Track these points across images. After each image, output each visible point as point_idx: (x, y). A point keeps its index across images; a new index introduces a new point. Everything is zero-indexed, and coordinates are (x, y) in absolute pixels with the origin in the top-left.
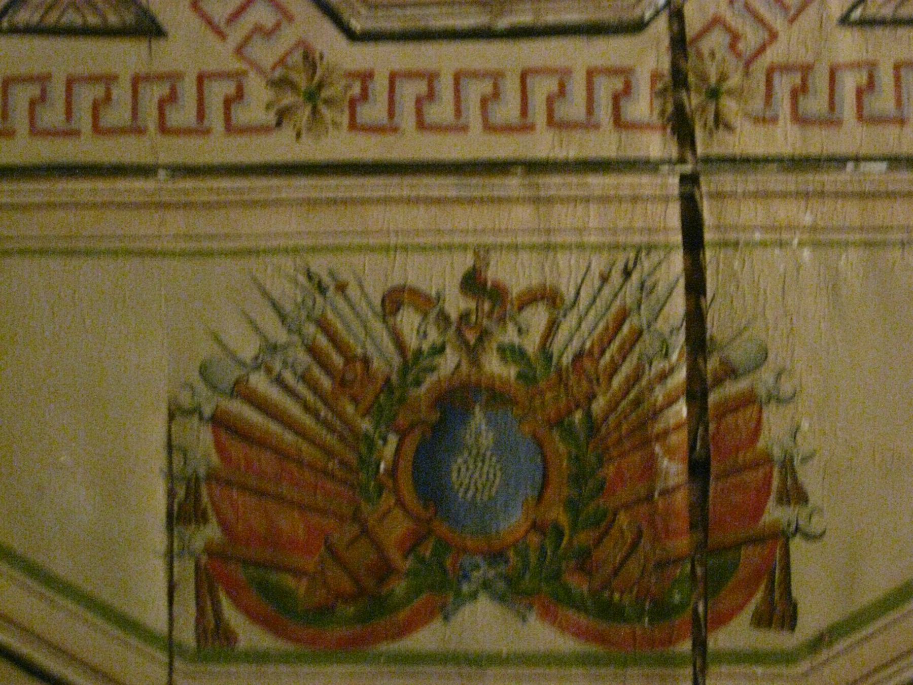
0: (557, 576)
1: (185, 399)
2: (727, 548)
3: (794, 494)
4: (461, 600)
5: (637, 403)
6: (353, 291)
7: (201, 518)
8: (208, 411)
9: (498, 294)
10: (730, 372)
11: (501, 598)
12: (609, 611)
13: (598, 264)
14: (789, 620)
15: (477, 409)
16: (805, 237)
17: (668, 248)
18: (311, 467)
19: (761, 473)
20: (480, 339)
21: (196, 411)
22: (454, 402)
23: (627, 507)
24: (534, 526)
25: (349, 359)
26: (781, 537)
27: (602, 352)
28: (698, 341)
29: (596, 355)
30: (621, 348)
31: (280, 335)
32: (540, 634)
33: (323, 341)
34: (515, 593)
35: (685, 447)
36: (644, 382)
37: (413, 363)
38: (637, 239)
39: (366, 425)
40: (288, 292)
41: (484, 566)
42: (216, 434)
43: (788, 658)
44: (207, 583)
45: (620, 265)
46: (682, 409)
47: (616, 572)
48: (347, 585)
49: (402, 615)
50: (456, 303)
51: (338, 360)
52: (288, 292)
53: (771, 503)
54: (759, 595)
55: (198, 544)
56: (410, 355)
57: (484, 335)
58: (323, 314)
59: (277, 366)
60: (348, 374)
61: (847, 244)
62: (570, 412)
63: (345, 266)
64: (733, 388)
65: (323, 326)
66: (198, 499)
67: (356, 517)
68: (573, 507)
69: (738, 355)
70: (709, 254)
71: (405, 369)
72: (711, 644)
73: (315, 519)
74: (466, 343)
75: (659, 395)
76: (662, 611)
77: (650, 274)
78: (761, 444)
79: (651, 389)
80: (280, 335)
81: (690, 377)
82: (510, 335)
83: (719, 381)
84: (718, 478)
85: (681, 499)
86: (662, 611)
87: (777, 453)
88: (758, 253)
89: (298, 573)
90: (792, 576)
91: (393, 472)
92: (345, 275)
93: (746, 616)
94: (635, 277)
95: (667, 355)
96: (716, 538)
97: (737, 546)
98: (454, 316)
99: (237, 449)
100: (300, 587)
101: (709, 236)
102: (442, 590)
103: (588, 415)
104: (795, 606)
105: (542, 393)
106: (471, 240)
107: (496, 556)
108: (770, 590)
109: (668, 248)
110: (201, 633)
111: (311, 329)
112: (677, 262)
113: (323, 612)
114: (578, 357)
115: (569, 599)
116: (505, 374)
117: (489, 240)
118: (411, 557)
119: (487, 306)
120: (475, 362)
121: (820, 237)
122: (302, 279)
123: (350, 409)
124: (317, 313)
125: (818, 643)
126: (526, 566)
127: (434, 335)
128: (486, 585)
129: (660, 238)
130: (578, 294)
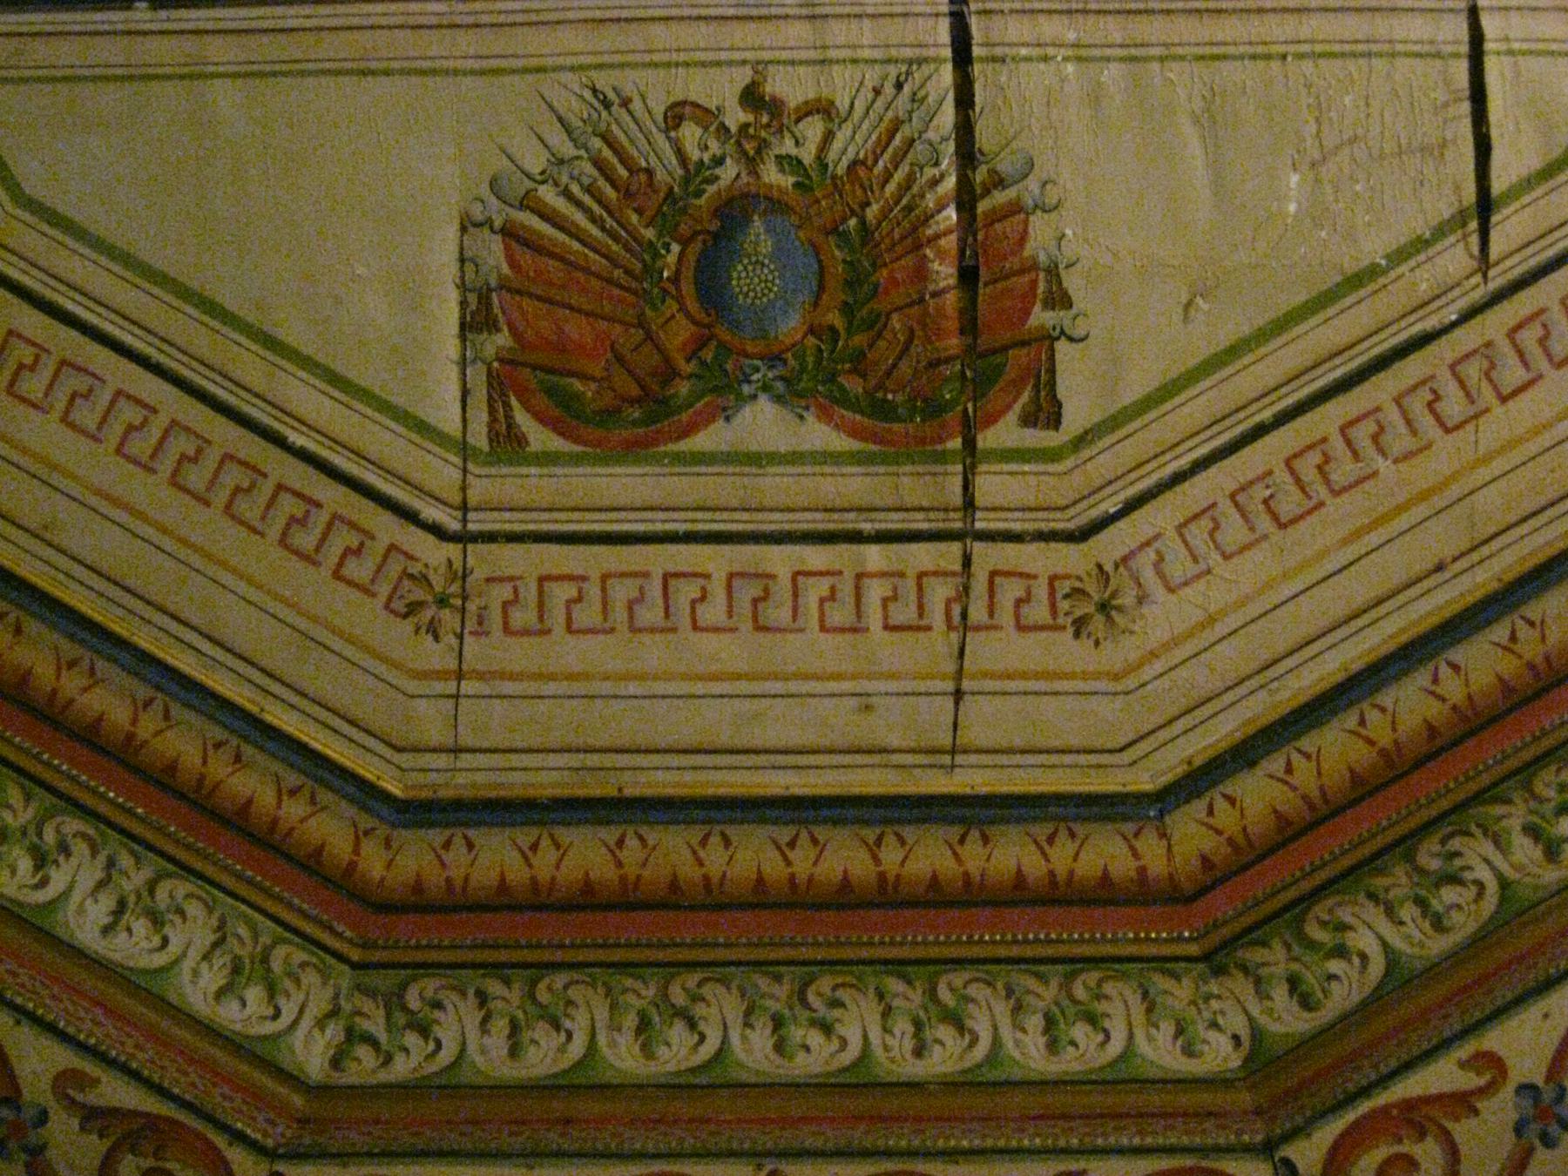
0: (832, 378)
1: (477, 213)
2: (994, 352)
3: (1060, 299)
4: (742, 400)
5: (909, 209)
6: (637, 105)
7: (492, 326)
8: (498, 224)
9: (774, 107)
10: (999, 182)
11: (779, 399)
12: (883, 411)
13: (872, 76)
14: (1055, 421)
15: (756, 218)
16: (1070, 53)
17: (938, 60)
18: (598, 276)
19: (1026, 278)
20: (759, 151)
21: (489, 222)
22: (735, 211)
23: (898, 309)
24: (811, 330)
25: (633, 170)
26: (1048, 339)
27: (876, 162)
28: (967, 154)
29: (869, 163)
30: (895, 155)
31: (568, 150)
32: (818, 434)
33: (607, 153)
34: (791, 394)
35: (954, 252)
36: (915, 189)
37: (695, 174)
38: (908, 53)
39: (649, 234)
40: (574, 108)
41: (763, 369)
42: (507, 248)
43: (1053, 455)
44: (499, 386)
45: (892, 79)
46: (951, 214)
47: (889, 373)
48: (635, 391)
49: (685, 417)
50: (736, 117)
51: (624, 173)
52: (574, 108)
53: (1037, 308)
54: (1025, 397)
55: (490, 351)
56: (691, 167)
57: (763, 146)
58: (608, 130)
59: (564, 179)
60: (628, 184)
61: (1108, 59)
62: (844, 220)
63: (629, 82)
64: (1000, 197)
65: (608, 139)
66: (489, 305)
67: (641, 323)
68: (847, 310)
69: (1005, 166)
70: (977, 68)
71: (687, 180)
72: (980, 444)
73: (603, 325)
74: (745, 153)
75: (930, 201)
76: (934, 409)
77: (922, 86)
78: (1027, 253)
79: (923, 196)
80: (568, 150)
81: (959, 181)
82: (788, 147)
83: (987, 192)
84: (986, 285)
85: (951, 300)
86: (934, 409)
87: (1042, 258)
88: (1023, 66)
89: (584, 377)
90: (1234, 457)
91: (675, 279)
92: (629, 90)
93: (1012, 417)
94: (907, 89)
95: (937, 164)
96: (984, 342)
97: (1005, 348)
98: (733, 129)
99: (526, 258)
100: (587, 390)
101: (976, 51)
102: (724, 392)
103: (863, 222)
104: (1060, 406)
105: (817, 201)
106: (749, 55)
107: (774, 359)
108: (1036, 387)
109: (942, 61)
110: (494, 436)
111: (597, 143)
112: (947, 75)
113: (608, 415)
114: (854, 164)
115: (845, 401)
116: (783, 184)
117: (766, 55)
118: (694, 362)
119: (765, 119)
120: (754, 173)
121: (1083, 52)
122: (588, 94)
123: (634, 218)
124: (603, 126)
125: (1080, 441)
126: (803, 370)
127: (715, 147)
128: (766, 388)
129: (931, 52)
130: (852, 104)
